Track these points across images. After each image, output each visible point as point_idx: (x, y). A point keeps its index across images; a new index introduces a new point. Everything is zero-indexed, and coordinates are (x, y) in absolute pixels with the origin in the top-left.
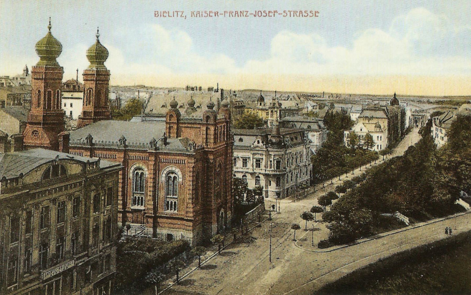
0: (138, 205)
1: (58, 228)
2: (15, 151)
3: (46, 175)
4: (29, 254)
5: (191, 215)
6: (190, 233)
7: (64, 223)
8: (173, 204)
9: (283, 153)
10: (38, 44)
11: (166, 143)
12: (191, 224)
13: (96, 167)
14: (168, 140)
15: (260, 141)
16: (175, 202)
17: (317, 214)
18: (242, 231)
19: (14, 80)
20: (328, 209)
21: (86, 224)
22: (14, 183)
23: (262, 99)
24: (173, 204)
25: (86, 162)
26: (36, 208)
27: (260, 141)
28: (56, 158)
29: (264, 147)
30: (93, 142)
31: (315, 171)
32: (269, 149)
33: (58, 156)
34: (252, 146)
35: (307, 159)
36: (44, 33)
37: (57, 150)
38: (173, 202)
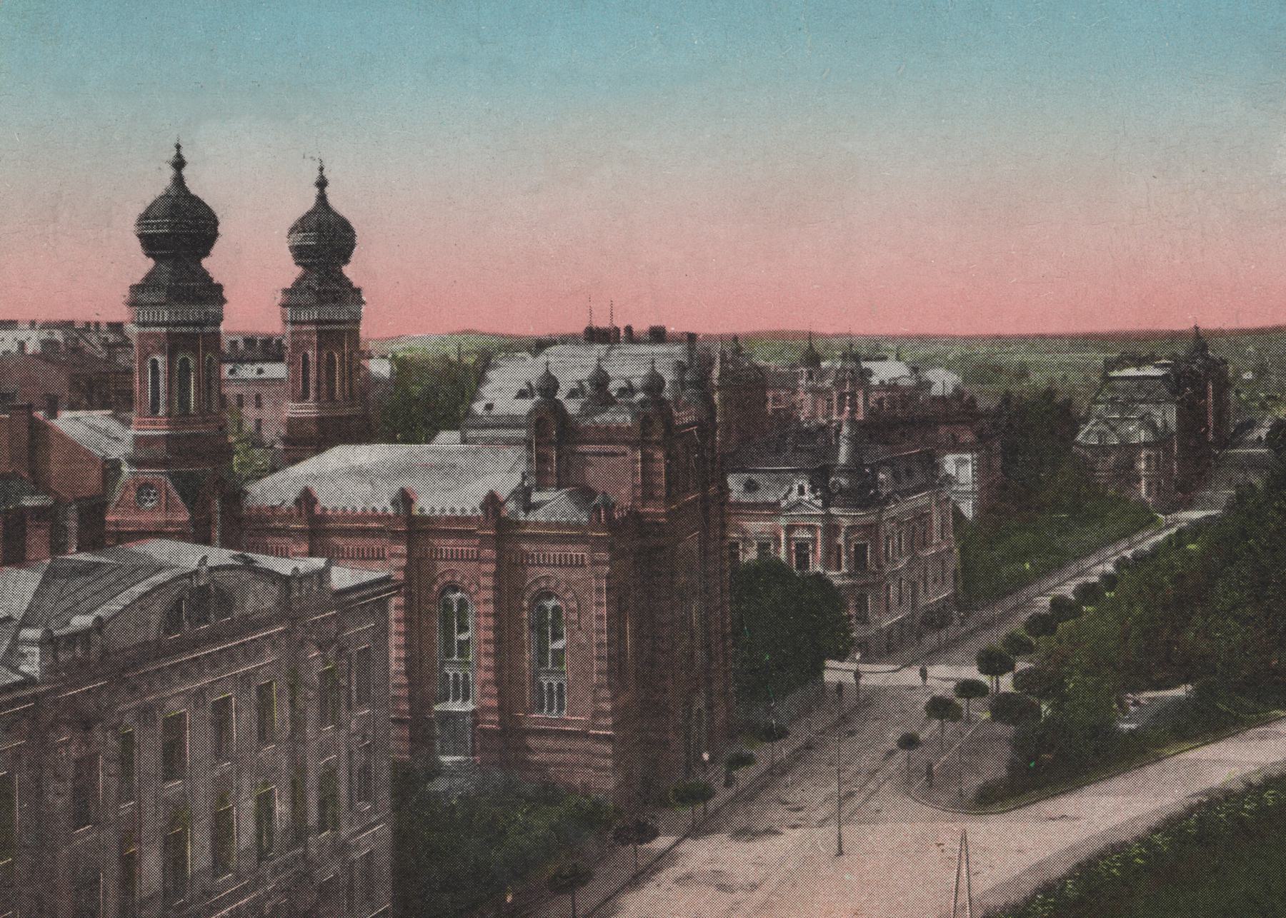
0: (455, 699)
1: (214, 780)
2: (79, 550)
3: (172, 619)
4: (129, 865)
5: (609, 721)
6: (607, 777)
7: (930, 495)
8: (555, 689)
9: (873, 518)
10: (144, 219)
11: (529, 507)
12: (608, 749)
13: (320, 587)
14: (536, 497)
15: (806, 487)
16: (560, 686)
17: (976, 703)
18: (1243, 102)
19: (89, 331)
20: (1006, 683)
21: (299, 769)
22: (78, 650)
23: (813, 359)
24: (555, 689)
25: (289, 573)
26: (197, 707)
27: (806, 487)
28: (200, 565)
29: (819, 503)
30: (318, 510)
31: (967, 575)
32: (833, 511)
33: (205, 558)
34: (784, 504)
35: (942, 537)
36: (159, 182)
37: (207, 541)
38: (555, 684)
